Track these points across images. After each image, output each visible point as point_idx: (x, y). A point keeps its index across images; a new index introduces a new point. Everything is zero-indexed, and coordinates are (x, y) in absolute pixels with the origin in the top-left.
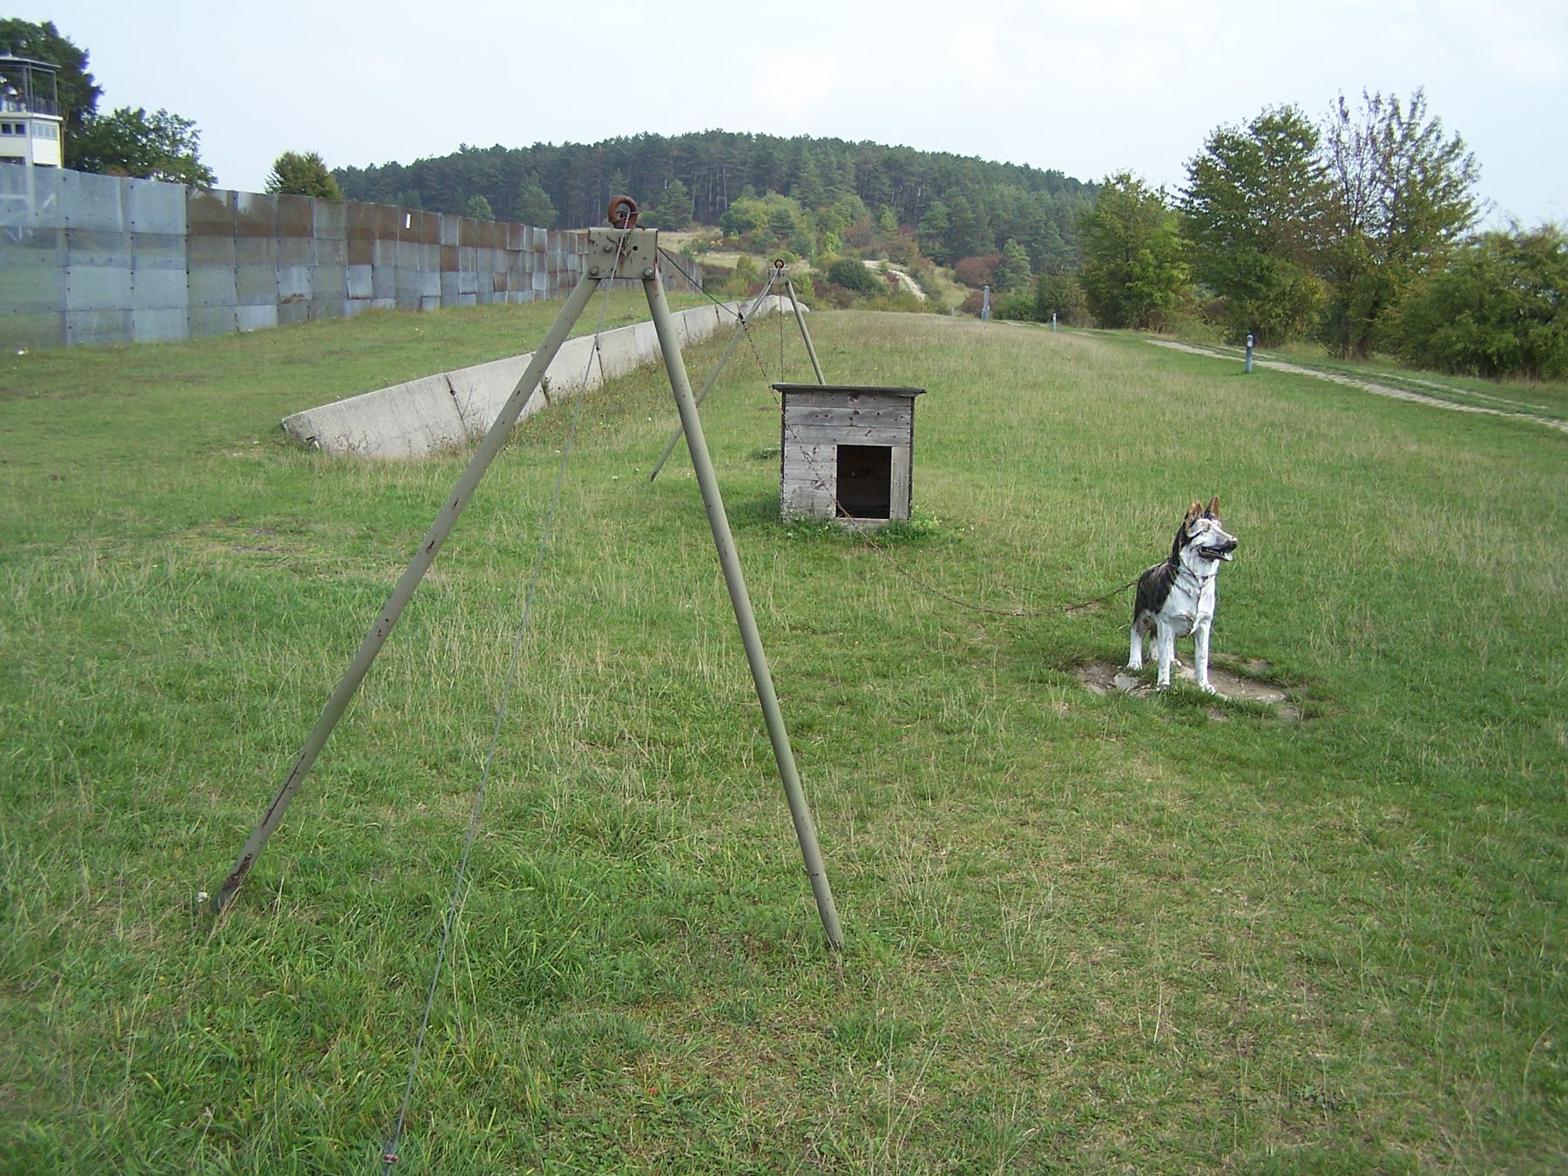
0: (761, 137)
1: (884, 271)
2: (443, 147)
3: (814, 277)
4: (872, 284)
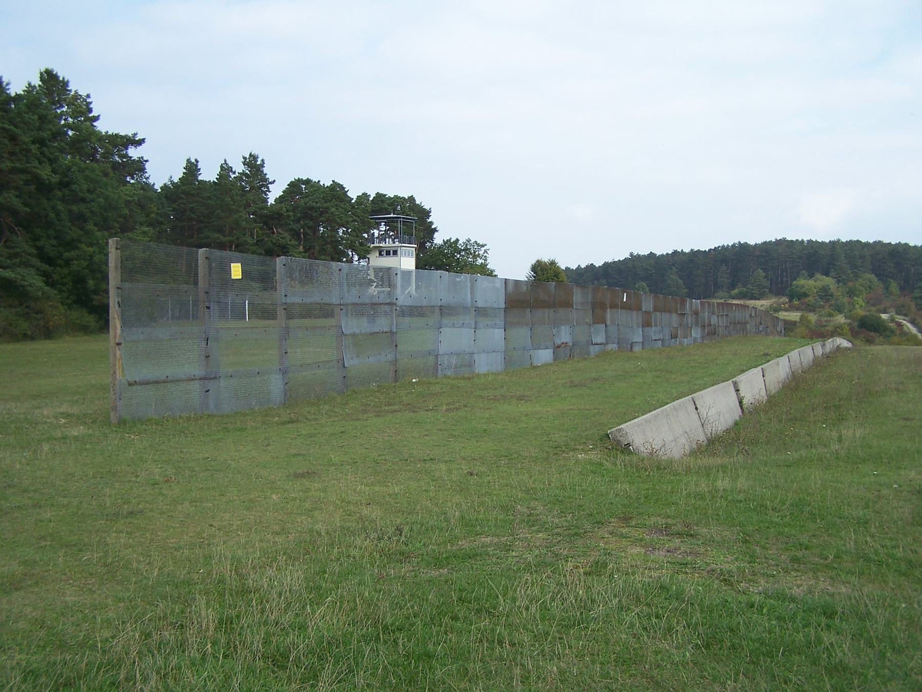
0: (810, 242)
1: (892, 320)
2: (620, 255)
3: (850, 324)
4: (886, 329)
